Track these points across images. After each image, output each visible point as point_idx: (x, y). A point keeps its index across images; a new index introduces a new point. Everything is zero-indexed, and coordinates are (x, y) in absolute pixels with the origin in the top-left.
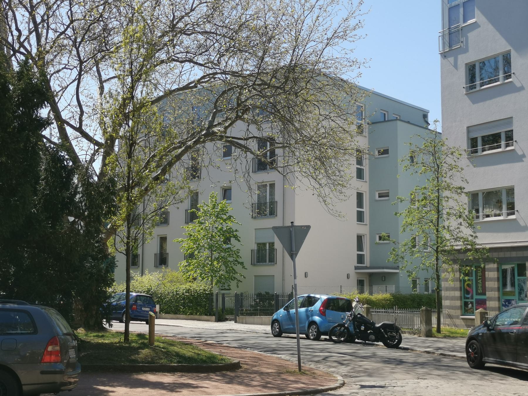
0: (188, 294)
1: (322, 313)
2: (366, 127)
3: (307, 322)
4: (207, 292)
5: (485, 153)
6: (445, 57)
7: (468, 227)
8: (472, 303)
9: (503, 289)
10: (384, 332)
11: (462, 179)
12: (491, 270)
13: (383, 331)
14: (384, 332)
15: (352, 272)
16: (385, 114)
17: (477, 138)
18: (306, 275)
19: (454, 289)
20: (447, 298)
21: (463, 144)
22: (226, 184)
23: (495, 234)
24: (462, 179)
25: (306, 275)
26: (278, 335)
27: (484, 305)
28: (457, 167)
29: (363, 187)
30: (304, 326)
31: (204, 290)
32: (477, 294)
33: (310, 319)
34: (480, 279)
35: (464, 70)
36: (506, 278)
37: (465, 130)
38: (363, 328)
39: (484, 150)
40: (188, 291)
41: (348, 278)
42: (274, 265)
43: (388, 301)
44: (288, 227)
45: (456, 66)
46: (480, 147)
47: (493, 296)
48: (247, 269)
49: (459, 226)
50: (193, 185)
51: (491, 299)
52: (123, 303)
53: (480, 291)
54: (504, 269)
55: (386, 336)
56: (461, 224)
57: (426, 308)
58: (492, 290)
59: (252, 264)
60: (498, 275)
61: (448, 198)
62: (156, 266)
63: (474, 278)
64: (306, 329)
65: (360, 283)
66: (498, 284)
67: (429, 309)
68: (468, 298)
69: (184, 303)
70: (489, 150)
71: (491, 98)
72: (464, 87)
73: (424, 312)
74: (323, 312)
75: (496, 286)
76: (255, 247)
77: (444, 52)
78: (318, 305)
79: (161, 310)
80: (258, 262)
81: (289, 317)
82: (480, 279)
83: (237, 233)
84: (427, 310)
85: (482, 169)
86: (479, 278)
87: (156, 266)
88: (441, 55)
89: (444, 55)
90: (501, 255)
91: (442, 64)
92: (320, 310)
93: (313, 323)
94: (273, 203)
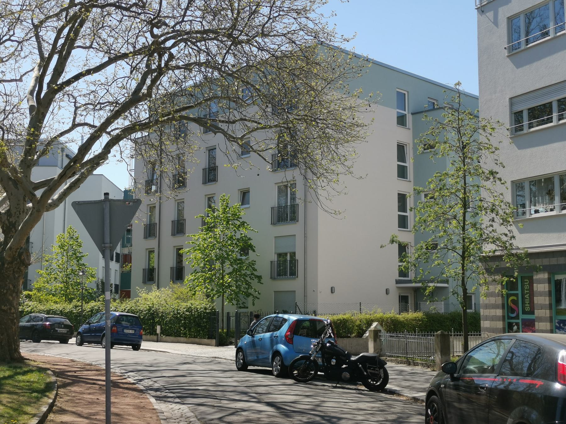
0: (188, 313)
1: (288, 341)
2: (409, 119)
3: (271, 352)
4: (207, 311)
5: (532, 129)
6: (483, 12)
7: (502, 224)
8: (517, 324)
9: (556, 306)
10: (362, 368)
11: (496, 162)
12: (540, 282)
13: (360, 366)
14: (362, 368)
15: (392, 286)
16: (434, 103)
17: (522, 111)
18: (332, 290)
19: (494, 307)
20: (487, 318)
21: (506, 119)
22: (244, 186)
23: (545, 235)
24: (496, 162)
25: (332, 290)
26: (243, 367)
27: (532, 327)
28: (491, 147)
29: (406, 187)
30: (268, 358)
31: (206, 309)
32: (524, 312)
33: (275, 348)
34: (527, 293)
35: (506, 27)
36: (560, 291)
37: (507, 103)
38: (334, 362)
39: (531, 126)
40: (189, 310)
41: (387, 294)
42: (295, 279)
43: (420, 321)
44: (100, 202)
45: (496, 22)
46: (526, 123)
47: (544, 315)
48: (262, 284)
49: (491, 223)
50: (210, 188)
51: (541, 319)
52: (103, 325)
53: (528, 309)
54: (558, 280)
55: (365, 373)
56: (493, 221)
57: (442, 332)
58: (542, 307)
59: (271, 278)
60: (550, 287)
61: (478, 186)
62: (144, 282)
63: (519, 292)
64: (270, 360)
65: (403, 300)
66: (550, 300)
67: (446, 333)
68: (512, 318)
69: (185, 323)
70: (537, 126)
71: (538, 58)
72: (505, 48)
73: (439, 338)
74: (289, 339)
75: (547, 302)
76: (275, 258)
77: (481, 6)
78: (285, 328)
79: (162, 332)
80: (279, 275)
81: (253, 344)
82: (527, 293)
83: (251, 241)
84: (442, 335)
85: (528, 151)
86: (526, 291)
87: (144, 282)
88: (478, 11)
89: (481, 10)
90: (554, 261)
91: (479, 22)
92: (286, 336)
93: (277, 353)
94: (294, 208)
